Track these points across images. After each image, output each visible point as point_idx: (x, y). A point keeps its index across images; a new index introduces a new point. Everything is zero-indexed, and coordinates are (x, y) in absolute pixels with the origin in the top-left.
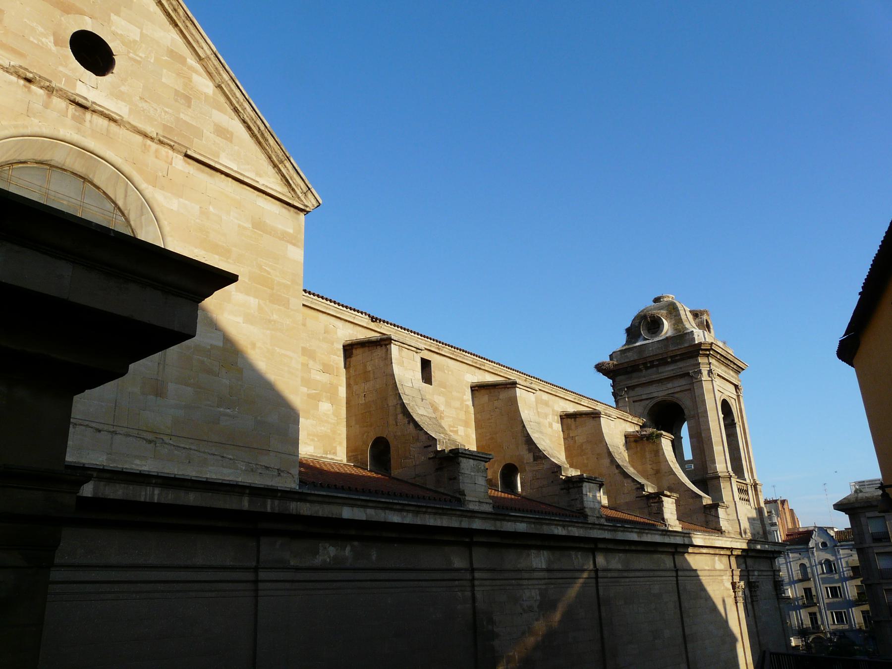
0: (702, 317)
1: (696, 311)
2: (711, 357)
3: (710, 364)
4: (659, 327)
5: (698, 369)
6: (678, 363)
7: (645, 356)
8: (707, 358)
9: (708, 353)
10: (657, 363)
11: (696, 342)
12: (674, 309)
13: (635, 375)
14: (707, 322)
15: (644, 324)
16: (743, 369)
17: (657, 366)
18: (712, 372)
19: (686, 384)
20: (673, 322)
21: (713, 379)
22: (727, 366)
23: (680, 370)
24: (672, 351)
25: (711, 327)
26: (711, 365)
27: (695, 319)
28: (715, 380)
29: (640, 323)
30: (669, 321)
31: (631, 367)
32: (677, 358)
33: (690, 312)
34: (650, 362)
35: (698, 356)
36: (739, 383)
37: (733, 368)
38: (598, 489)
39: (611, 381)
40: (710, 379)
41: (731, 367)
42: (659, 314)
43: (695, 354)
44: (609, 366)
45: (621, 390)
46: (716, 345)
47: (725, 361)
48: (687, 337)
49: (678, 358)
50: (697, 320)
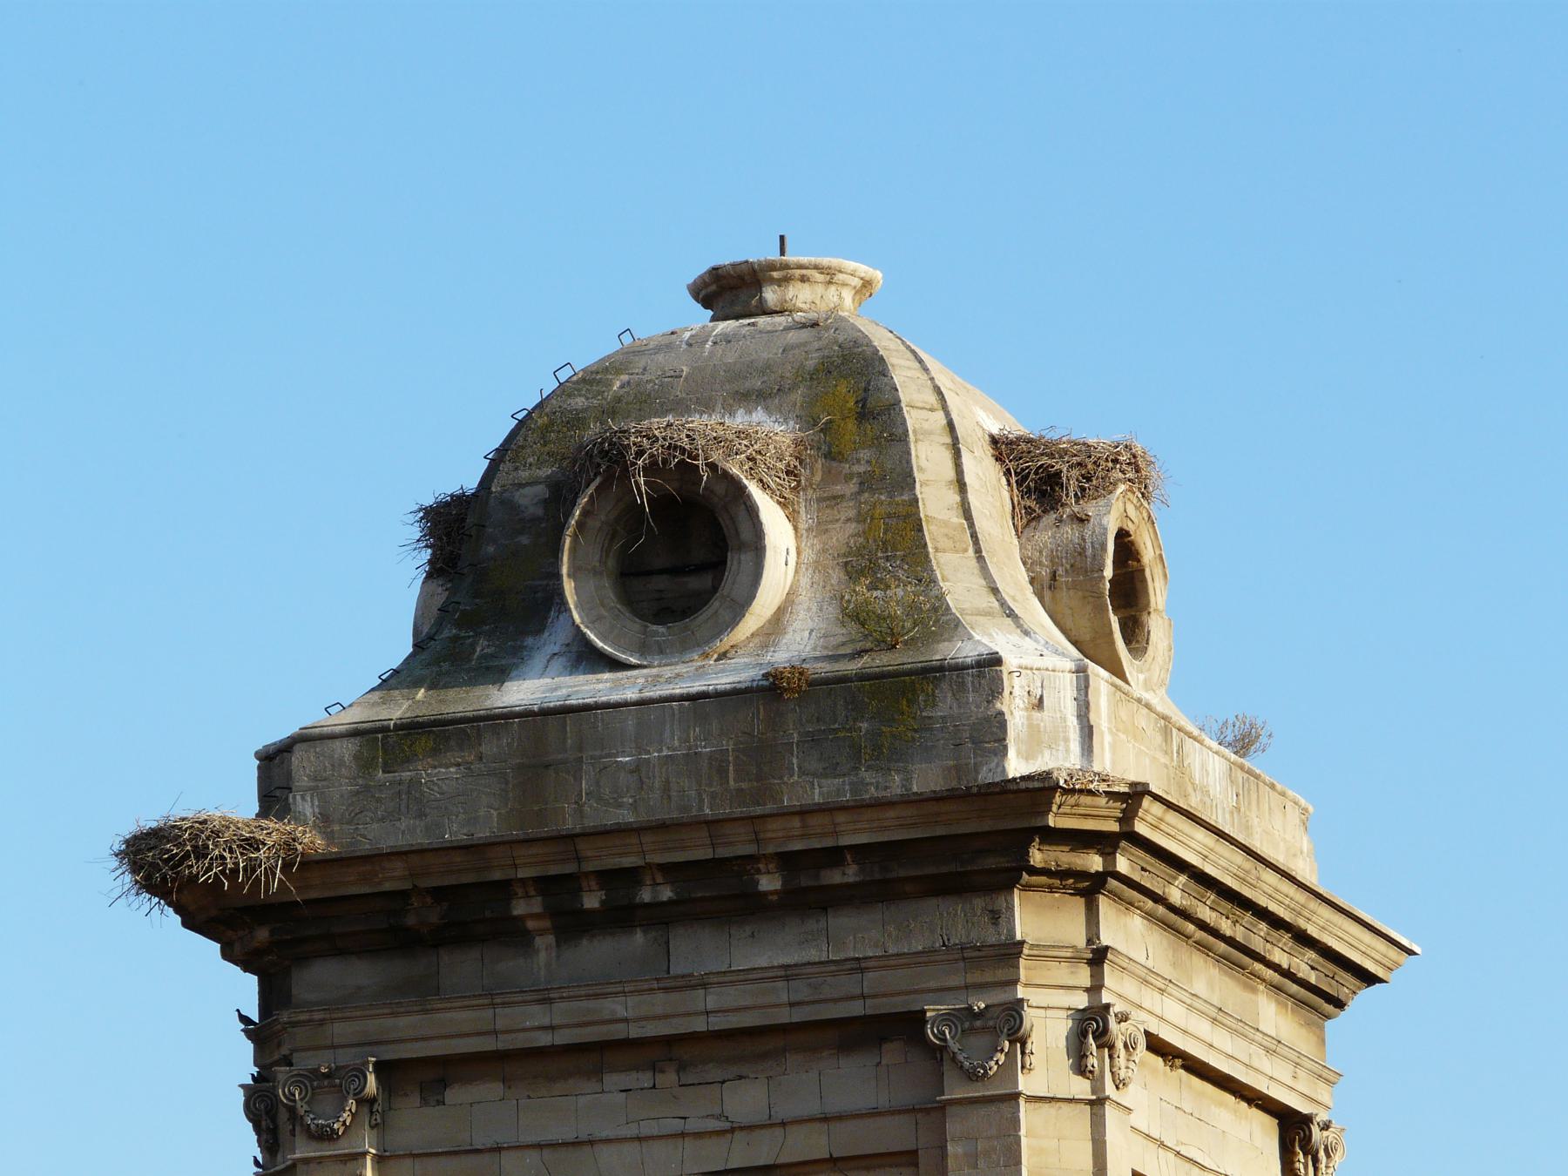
0: (1091, 508)
1: (1052, 449)
2: (1117, 897)
3: (1098, 957)
4: (717, 566)
5: (998, 997)
6: (841, 921)
7: (570, 824)
8: (1079, 903)
9: (1095, 863)
10: (666, 894)
11: (1016, 766)
12: (864, 414)
13: (460, 966)
14: (1126, 547)
15: (595, 524)
16: (1369, 979)
17: (661, 918)
18: (1102, 1035)
19: (883, 1102)
20: (843, 533)
21: (1110, 1089)
22: (1237, 959)
23: (848, 984)
24: (804, 812)
25: (1158, 593)
26: (1110, 976)
27: (1026, 520)
28: (1126, 1097)
29: (560, 496)
30: (805, 520)
31: (438, 893)
32: (835, 877)
33: (1002, 447)
34: (610, 878)
35: (1008, 887)
36: (1323, 1093)
37: (1288, 974)
38: (541, 672)
39: (251, 982)
40: (1081, 1087)
41: (1276, 967)
42: (731, 452)
43: (991, 862)
44: (252, 867)
45: (340, 1081)
46: (1170, 805)
47: (1226, 927)
48: (945, 705)
49: (849, 874)
50: (1046, 535)
